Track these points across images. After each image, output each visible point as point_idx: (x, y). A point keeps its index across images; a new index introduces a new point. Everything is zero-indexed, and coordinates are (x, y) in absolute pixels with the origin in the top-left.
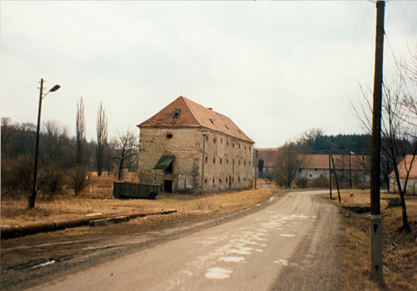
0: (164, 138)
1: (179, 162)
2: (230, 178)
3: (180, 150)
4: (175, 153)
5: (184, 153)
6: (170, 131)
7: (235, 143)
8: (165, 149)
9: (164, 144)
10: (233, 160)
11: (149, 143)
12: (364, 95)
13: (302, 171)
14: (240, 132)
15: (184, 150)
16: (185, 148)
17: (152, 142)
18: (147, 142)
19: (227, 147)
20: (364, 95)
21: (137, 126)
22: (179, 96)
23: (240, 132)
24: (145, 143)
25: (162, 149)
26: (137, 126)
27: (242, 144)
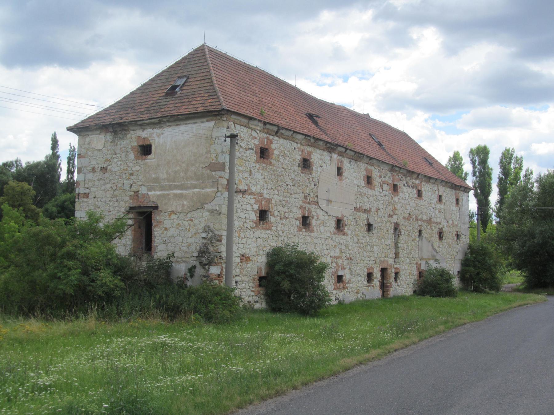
0: (132, 156)
1: (167, 223)
2: (383, 271)
3: (170, 188)
4: (159, 196)
5: (181, 196)
6: (145, 134)
7: (400, 184)
8: (135, 188)
9: (131, 174)
10: (396, 228)
11: (98, 175)
12: (520, 306)
13: (261, 288)
14: (431, 164)
15: (182, 187)
16: (185, 182)
17: (104, 169)
18: (94, 170)
19: (366, 190)
20: (520, 306)
21: (70, 129)
22: (197, 44)
23: (431, 164)
24: (90, 176)
25: (128, 188)
26: (70, 129)
27: (426, 188)
